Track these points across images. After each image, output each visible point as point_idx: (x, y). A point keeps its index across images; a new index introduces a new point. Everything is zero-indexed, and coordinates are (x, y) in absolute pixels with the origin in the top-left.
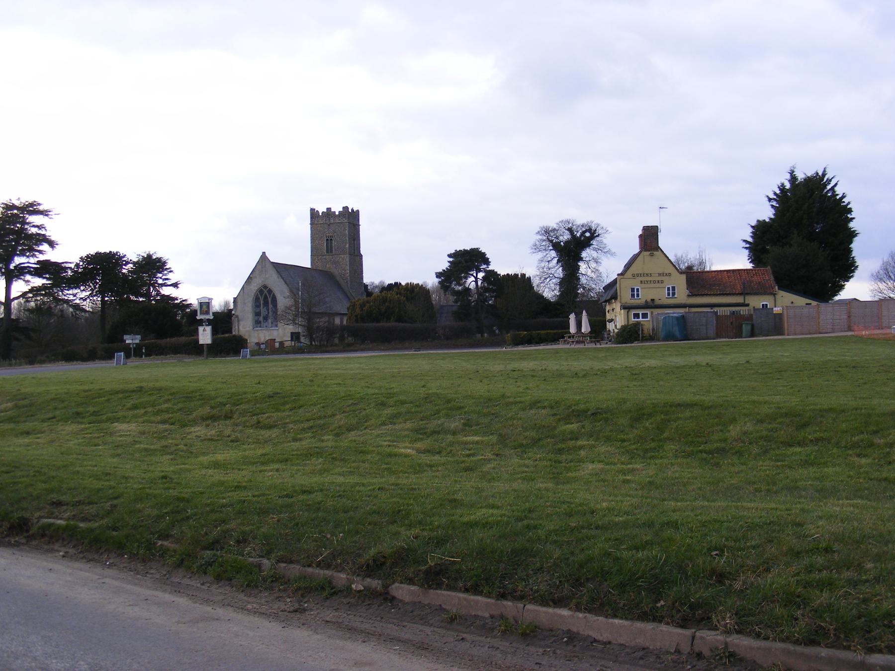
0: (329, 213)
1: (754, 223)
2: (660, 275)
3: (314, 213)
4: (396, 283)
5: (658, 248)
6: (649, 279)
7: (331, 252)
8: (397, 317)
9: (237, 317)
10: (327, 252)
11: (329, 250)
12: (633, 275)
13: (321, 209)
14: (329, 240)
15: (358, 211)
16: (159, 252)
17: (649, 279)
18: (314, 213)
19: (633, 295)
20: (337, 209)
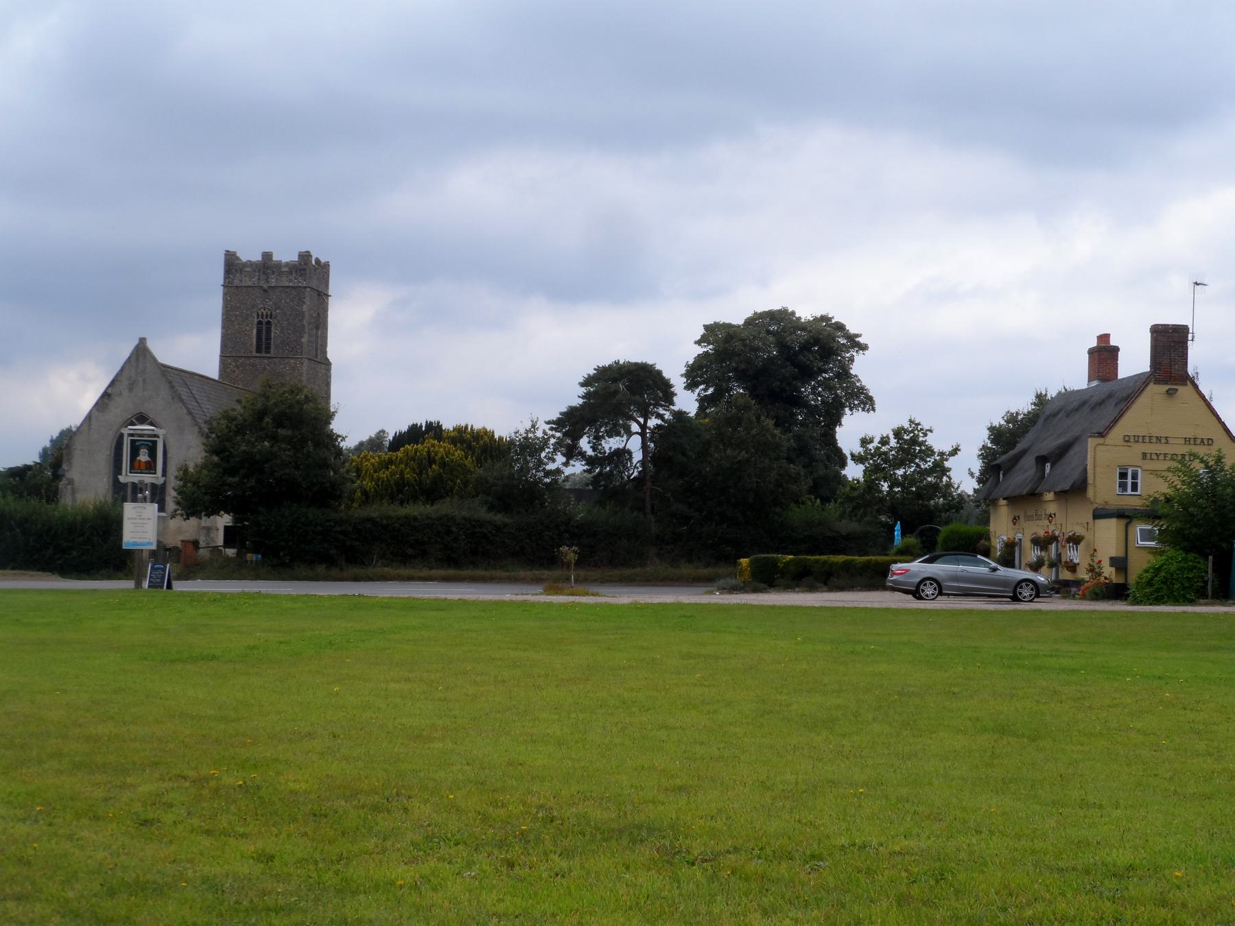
0: (267, 265)
1: (683, 370)
2: (1187, 441)
3: (232, 264)
4: (430, 426)
5: (1185, 379)
6: (1162, 448)
7: (268, 350)
8: (461, 509)
9: (71, 482)
10: (259, 350)
11: (263, 344)
12: (1127, 439)
13: (250, 254)
14: (264, 328)
15: (327, 265)
16: (319, 253)
17: (1162, 448)
18: (232, 264)
19: (1123, 486)
20: (286, 255)
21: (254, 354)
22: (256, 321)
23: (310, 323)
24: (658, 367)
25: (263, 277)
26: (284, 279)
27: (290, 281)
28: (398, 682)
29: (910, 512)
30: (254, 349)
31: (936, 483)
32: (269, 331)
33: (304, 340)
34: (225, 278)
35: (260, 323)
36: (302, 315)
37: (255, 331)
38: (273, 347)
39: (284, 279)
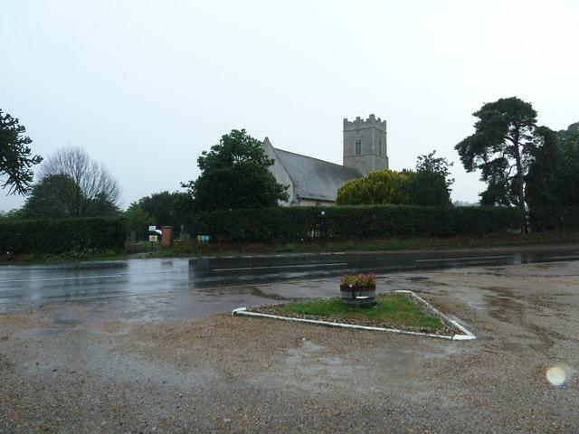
3: (346, 122)
11: (358, 151)
36: (370, 138)
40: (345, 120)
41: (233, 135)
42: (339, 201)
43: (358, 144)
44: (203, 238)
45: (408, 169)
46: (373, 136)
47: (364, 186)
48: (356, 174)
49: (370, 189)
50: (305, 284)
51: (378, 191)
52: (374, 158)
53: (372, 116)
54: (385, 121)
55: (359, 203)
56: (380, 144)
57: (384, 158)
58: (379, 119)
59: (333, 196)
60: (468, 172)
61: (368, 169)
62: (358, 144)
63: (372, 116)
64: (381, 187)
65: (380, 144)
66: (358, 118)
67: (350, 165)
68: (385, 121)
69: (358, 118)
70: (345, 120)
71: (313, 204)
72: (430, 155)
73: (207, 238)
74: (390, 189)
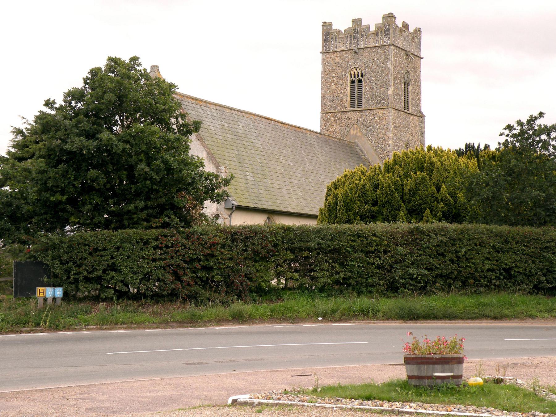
0: (357, 29)
3: (328, 34)
7: (360, 104)
10: (352, 105)
11: (356, 100)
21: (349, 109)
22: (349, 79)
23: (395, 78)
24: (146, 65)
25: (354, 41)
26: (371, 40)
27: (377, 41)
28: (28, 391)
29: (362, 398)
30: (348, 105)
31: (175, 280)
32: (360, 88)
33: (390, 92)
34: (323, 46)
35: (353, 82)
36: (385, 71)
37: (348, 89)
38: (364, 102)
39: (371, 40)
40: (327, 28)
41: (110, 69)
42: (332, 211)
43: (357, 82)
44: (49, 292)
45: (479, 142)
46: (390, 65)
47: (386, 179)
48: (350, 149)
49: (399, 187)
50: (172, 377)
51: (413, 193)
52: (391, 115)
53: (390, 17)
54: (418, 31)
55: (374, 218)
56: (407, 84)
57: (410, 107)
58: (406, 26)
59: (316, 204)
60: (520, 120)
61: (382, 146)
62: (357, 82)
63: (390, 17)
64: (420, 184)
65: (407, 84)
66: (357, 22)
67: (337, 130)
68: (418, 31)
69: (357, 22)
70: (327, 28)
71: (259, 220)
72: (532, 120)
73: (59, 292)
74: (438, 189)
